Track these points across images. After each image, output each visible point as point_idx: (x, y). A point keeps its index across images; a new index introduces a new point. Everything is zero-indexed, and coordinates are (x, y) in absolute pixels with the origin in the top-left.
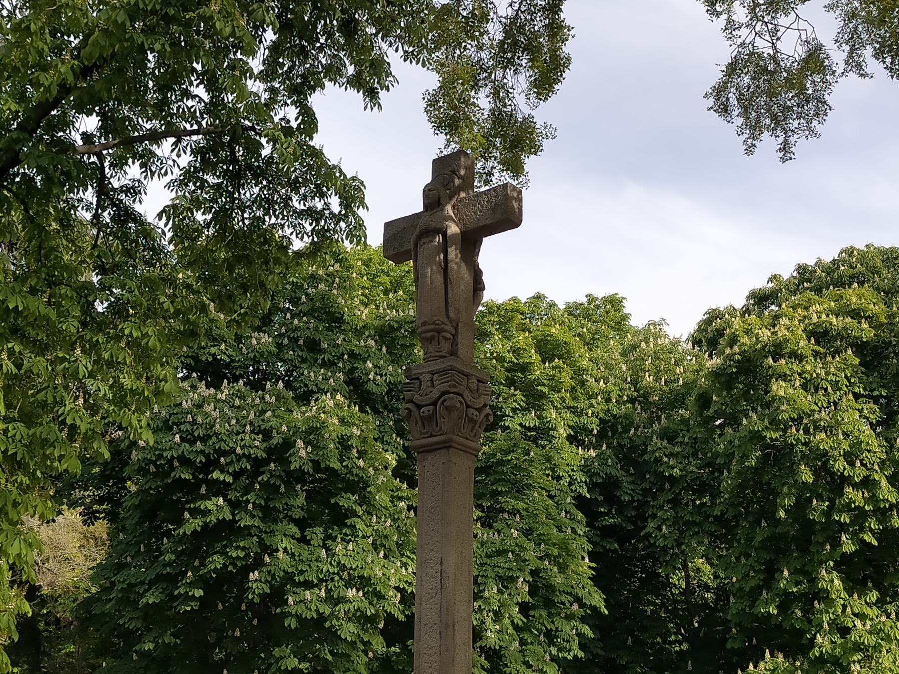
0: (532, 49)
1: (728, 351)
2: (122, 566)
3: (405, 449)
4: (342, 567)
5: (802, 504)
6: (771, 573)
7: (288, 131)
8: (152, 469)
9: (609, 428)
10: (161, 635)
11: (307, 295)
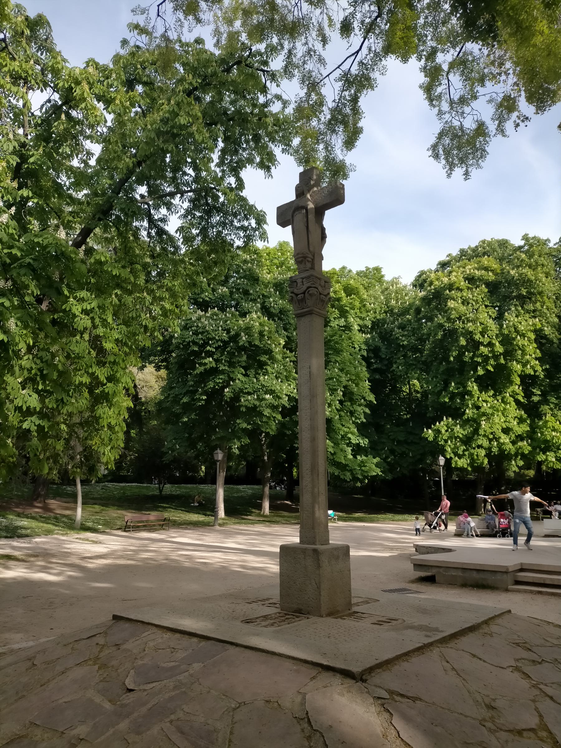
0: (345, 123)
1: (429, 288)
2: (171, 388)
3: (287, 337)
4: (263, 386)
5: (461, 355)
6: (447, 384)
7: (231, 189)
8: (181, 346)
9: (376, 325)
10: (190, 415)
11: (243, 269)
